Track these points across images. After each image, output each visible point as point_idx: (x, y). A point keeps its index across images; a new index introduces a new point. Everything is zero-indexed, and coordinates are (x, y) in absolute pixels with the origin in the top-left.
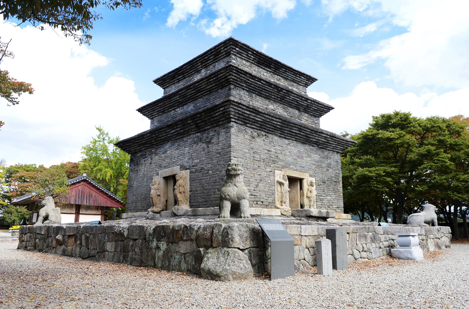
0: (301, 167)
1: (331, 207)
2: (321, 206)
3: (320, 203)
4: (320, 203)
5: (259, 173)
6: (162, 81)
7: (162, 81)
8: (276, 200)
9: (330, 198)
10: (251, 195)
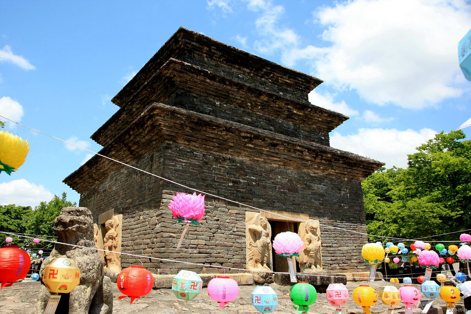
0: (294, 204)
1: (349, 262)
2: (331, 262)
3: (330, 258)
4: (330, 258)
5: (216, 218)
6: (96, 137)
7: (96, 137)
8: (248, 258)
9: (346, 248)
10: (200, 253)
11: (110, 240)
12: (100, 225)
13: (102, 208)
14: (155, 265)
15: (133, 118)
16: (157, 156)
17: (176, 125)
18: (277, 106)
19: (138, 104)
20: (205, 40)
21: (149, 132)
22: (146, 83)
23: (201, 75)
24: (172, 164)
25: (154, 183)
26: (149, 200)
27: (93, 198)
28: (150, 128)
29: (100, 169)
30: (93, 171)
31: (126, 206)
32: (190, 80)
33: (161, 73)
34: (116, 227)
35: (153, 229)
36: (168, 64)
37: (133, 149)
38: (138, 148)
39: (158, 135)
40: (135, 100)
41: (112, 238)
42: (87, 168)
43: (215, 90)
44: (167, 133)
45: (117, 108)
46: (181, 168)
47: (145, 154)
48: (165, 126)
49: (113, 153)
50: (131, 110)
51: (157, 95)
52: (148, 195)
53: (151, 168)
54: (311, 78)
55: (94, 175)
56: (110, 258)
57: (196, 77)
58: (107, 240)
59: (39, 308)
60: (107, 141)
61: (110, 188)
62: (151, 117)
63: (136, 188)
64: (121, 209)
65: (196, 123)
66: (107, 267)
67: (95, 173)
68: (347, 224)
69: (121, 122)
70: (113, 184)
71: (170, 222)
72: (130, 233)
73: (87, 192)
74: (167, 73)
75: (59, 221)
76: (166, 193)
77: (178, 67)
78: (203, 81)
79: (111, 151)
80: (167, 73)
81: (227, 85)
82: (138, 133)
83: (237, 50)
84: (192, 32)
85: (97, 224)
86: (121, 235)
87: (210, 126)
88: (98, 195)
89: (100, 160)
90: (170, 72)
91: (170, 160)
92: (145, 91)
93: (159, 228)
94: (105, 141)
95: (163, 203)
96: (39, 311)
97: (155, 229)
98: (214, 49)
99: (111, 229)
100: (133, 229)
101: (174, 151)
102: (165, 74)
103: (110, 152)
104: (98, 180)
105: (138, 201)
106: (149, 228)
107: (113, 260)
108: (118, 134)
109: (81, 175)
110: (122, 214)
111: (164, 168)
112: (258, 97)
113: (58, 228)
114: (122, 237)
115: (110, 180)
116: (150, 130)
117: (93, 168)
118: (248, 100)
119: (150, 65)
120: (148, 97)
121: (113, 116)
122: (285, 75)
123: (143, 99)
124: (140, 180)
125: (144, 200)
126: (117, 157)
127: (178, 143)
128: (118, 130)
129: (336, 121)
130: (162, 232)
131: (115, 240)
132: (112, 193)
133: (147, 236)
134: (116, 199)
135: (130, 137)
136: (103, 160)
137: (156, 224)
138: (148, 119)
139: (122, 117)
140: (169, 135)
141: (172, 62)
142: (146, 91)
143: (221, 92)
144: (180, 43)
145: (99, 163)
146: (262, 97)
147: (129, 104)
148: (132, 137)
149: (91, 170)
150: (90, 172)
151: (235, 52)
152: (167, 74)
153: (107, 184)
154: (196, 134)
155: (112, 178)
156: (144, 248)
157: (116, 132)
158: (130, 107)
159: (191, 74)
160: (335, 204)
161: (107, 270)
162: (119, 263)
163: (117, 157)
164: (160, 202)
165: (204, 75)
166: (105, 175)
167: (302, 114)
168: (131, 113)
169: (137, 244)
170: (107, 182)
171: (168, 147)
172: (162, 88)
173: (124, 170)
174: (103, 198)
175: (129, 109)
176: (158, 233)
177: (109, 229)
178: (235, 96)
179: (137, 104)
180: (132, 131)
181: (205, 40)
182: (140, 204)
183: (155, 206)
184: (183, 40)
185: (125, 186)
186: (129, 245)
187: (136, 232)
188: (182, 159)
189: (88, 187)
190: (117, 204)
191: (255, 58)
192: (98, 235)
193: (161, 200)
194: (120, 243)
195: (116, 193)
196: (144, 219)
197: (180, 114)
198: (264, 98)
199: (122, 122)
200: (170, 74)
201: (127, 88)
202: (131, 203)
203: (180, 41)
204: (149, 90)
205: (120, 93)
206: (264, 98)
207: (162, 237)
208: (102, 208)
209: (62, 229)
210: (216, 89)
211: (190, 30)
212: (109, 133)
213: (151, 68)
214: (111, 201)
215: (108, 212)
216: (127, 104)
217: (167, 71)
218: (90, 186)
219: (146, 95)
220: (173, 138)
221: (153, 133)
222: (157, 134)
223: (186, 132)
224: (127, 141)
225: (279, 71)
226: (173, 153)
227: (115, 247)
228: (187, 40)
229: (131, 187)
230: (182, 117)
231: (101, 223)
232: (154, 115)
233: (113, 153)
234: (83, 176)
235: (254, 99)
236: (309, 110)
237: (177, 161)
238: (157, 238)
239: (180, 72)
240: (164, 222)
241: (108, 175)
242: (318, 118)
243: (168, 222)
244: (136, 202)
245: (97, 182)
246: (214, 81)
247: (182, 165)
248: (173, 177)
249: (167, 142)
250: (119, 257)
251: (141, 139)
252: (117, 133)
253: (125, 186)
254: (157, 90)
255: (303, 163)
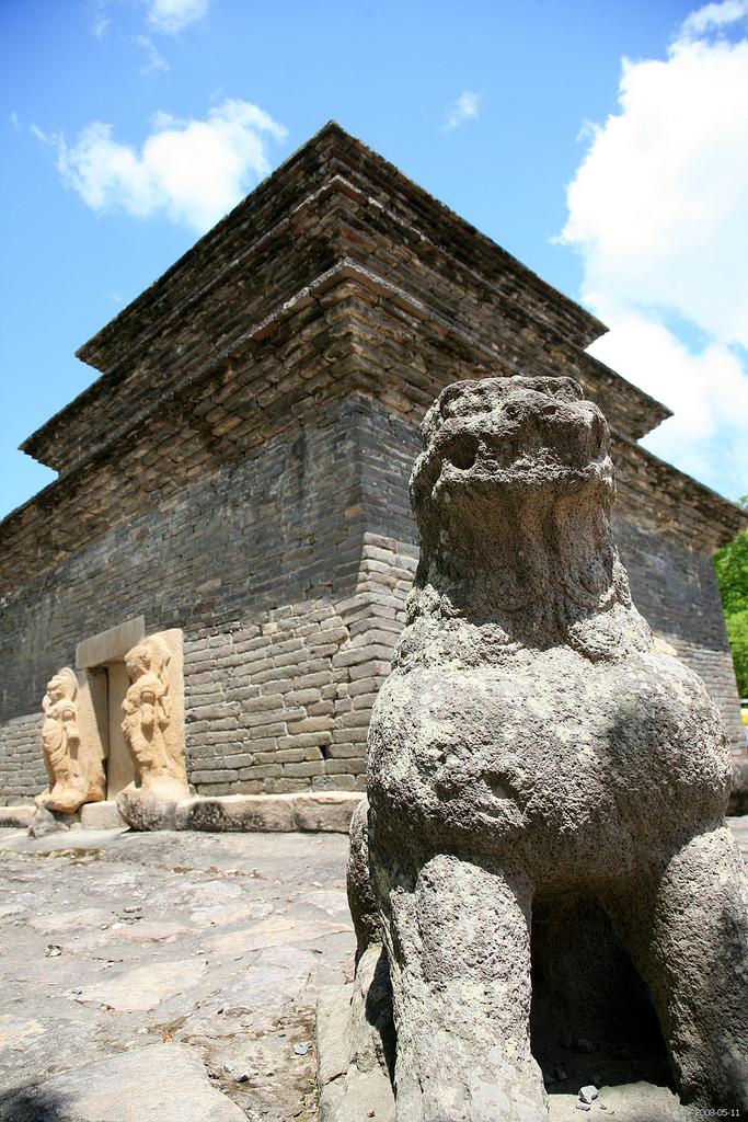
6: (35, 447)
11: (147, 706)
12: (84, 673)
13: (87, 621)
14: (352, 764)
15: (170, 376)
16: (321, 440)
17: (391, 342)
18: (551, 361)
19: (195, 332)
20: (385, 171)
21: (300, 365)
22: (237, 261)
23: (403, 242)
24: (378, 458)
25: (320, 516)
26: (301, 573)
27: (48, 601)
28: (307, 352)
29: (79, 513)
30: (52, 520)
31: (198, 601)
32: (373, 253)
33: (291, 227)
34: (161, 668)
35: (331, 656)
36: (325, 197)
37: (220, 431)
38: (240, 425)
39: (330, 373)
40: (188, 319)
41: (152, 699)
42: (35, 514)
43: (429, 294)
44: (366, 366)
45: (91, 375)
46: (399, 474)
47: (263, 442)
48: (361, 342)
49: (142, 452)
50: (170, 350)
51: (265, 299)
52: (295, 556)
53: (301, 476)
54: (589, 318)
55: (54, 533)
56: (149, 759)
57: (390, 246)
58: (136, 706)
59: (481, 1033)
60: (71, 456)
61: (118, 561)
62: (318, 313)
63: (235, 543)
64: (176, 612)
65: (440, 346)
66: (138, 785)
67: (59, 525)
68: (706, 651)
69: (127, 391)
70: (131, 549)
71: (393, 629)
72: (220, 680)
73: (22, 589)
74: (315, 226)
75: (534, 416)
76: (374, 543)
77: (352, 210)
78: (405, 262)
79: (134, 448)
80: (315, 226)
81: (457, 283)
82: (256, 373)
83: (454, 213)
84: (356, 141)
85: (73, 668)
86: (182, 689)
87: (469, 360)
88: (66, 588)
89: (88, 483)
90: (324, 221)
91: (373, 446)
92: (229, 286)
93: (362, 649)
94: (64, 455)
95: (368, 571)
96: (495, 1055)
97: (340, 653)
98: (402, 201)
99: (144, 673)
100: (234, 666)
101: (378, 424)
102: (307, 229)
103: (127, 452)
104: (65, 548)
105: (252, 581)
106: (312, 652)
107: (157, 762)
108: (110, 430)
109: (7, 538)
110: (181, 627)
111: (359, 470)
112: (517, 332)
113: (526, 468)
114: (186, 695)
115: (116, 539)
116: (307, 357)
117: (55, 511)
118: (494, 336)
119: (214, 241)
120: (232, 308)
121: (78, 399)
122: (541, 301)
123: (215, 315)
124: (251, 520)
125: (279, 572)
126: (153, 465)
127: (386, 404)
128: (112, 419)
129: (651, 418)
130: (377, 659)
131: (161, 704)
132: (126, 575)
133: (299, 681)
134: (149, 587)
135: (218, 392)
136: (98, 479)
137: (343, 639)
138: (308, 321)
139: (134, 375)
140: (367, 375)
141: (337, 188)
142: (232, 288)
143: (441, 302)
144: (322, 170)
145: (81, 492)
146: (525, 332)
147: (165, 333)
148: (226, 392)
149: (48, 519)
150: (43, 526)
151: (446, 219)
152: (313, 230)
153: (103, 554)
154: (433, 380)
155: (123, 533)
156: (295, 716)
157: (106, 423)
158: (167, 344)
159: (378, 235)
160: (683, 603)
161: (141, 796)
162: (182, 772)
163: (153, 465)
164: (356, 568)
165: (409, 246)
166: (94, 529)
167: (594, 390)
168: (165, 361)
169: (257, 709)
170: (105, 548)
171: (362, 410)
172: (286, 275)
173: (176, 502)
174: (90, 594)
175: (160, 350)
176: (356, 664)
177: (140, 673)
178: (469, 319)
179: (192, 331)
180: (234, 369)
181: (385, 171)
182: (261, 589)
183: (330, 585)
184: (334, 160)
185: (184, 548)
186: (222, 714)
187: (251, 674)
188: (397, 449)
189: (29, 572)
190: (154, 601)
191: (489, 243)
192: (77, 701)
193: (359, 564)
194: (180, 713)
195: (149, 570)
196: (287, 629)
197: (406, 311)
198: (529, 335)
199: (132, 393)
200: (324, 229)
201: (131, 311)
202: (219, 591)
203: (323, 164)
204: (240, 283)
205: (106, 330)
206: (529, 335)
207: (377, 675)
208: (87, 621)
209: (556, 471)
210: (431, 291)
211: (353, 136)
212: (82, 430)
213: (217, 248)
214: (128, 597)
215: (118, 633)
216: (159, 334)
217: (314, 220)
218: (33, 569)
219: (228, 303)
220: (375, 384)
221: (314, 368)
222: (329, 371)
223: (412, 372)
224: (203, 405)
225: (532, 287)
226: (377, 428)
227: (163, 726)
228: (341, 163)
229: (213, 545)
230: (410, 319)
231: (86, 666)
232: (335, 304)
233: (142, 452)
234: (15, 540)
235: (508, 334)
236: (610, 381)
237: (388, 453)
238: (349, 681)
239: (357, 226)
240: (377, 628)
241: (107, 527)
242: (622, 404)
243: (389, 628)
244: (241, 584)
245: (63, 553)
246: (432, 268)
247: (400, 466)
248: (386, 497)
249: (359, 393)
250: (178, 754)
251: (260, 394)
252: (111, 425)
253: (184, 548)
254: (271, 283)
255: (630, 498)
